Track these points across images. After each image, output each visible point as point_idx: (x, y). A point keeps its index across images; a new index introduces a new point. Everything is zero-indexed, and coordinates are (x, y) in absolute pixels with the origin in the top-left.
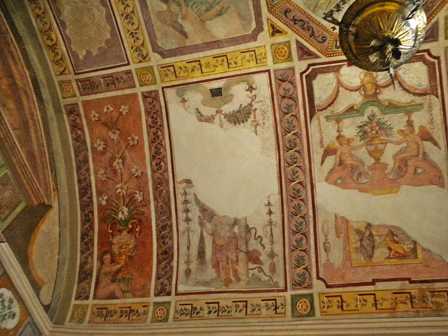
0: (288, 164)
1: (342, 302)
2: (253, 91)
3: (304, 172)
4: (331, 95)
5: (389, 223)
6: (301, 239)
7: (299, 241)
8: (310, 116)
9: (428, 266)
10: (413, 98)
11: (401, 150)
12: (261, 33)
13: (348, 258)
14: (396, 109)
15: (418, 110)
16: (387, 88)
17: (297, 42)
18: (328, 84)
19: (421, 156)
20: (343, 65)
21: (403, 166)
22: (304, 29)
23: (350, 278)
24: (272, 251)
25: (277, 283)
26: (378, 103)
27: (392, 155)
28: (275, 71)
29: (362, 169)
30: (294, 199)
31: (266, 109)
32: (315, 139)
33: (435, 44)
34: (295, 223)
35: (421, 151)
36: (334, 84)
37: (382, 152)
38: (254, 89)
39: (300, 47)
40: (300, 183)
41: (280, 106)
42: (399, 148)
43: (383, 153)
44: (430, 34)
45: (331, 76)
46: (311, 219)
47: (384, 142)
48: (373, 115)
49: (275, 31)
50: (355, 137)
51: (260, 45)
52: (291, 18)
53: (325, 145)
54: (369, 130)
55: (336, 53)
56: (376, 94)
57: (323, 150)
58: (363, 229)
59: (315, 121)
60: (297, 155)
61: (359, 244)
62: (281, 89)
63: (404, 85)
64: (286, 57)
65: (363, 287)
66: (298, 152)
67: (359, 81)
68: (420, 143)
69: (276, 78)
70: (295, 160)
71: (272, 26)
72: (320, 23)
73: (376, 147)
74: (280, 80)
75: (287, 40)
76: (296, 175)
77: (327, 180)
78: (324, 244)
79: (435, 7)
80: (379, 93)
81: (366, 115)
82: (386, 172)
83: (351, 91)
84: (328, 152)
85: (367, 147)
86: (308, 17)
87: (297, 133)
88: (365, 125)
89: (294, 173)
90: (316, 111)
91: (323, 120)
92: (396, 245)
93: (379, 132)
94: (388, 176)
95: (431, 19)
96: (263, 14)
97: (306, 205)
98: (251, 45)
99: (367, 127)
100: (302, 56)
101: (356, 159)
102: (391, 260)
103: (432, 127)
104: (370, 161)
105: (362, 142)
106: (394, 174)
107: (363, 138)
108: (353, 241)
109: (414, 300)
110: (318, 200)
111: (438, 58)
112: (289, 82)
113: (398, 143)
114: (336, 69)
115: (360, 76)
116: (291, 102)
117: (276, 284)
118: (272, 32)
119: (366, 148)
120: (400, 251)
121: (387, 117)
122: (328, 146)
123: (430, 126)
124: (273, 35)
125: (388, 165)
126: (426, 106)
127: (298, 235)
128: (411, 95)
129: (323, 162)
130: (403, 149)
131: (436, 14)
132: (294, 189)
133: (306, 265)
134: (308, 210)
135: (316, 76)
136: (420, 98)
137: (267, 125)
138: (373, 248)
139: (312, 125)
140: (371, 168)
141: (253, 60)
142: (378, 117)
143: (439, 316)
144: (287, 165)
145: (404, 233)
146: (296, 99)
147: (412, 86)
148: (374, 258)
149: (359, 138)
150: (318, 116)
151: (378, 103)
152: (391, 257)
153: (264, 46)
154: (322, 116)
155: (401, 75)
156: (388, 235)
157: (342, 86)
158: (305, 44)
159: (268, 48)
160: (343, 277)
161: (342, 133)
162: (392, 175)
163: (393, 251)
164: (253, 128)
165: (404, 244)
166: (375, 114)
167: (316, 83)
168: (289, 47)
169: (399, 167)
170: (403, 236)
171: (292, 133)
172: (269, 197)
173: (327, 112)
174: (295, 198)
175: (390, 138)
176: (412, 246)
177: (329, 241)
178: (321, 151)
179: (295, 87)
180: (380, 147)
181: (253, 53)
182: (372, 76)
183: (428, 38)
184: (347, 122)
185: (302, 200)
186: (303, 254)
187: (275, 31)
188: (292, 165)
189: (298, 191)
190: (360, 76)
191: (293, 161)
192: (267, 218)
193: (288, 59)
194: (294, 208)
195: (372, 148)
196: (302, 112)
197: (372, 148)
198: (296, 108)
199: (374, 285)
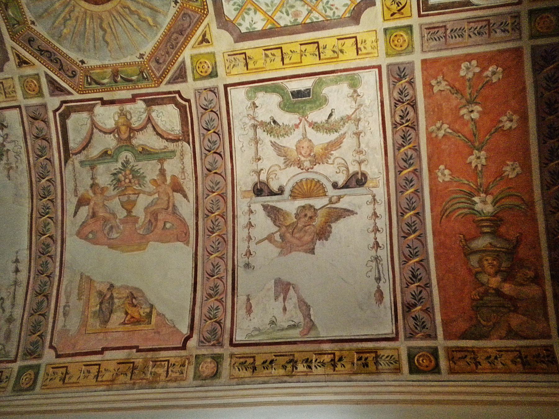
0: (41, 215)
1: (67, 373)
2: (5, 129)
3: (55, 223)
4: (85, 137)
5: (130, 285)
6: (42, 302)
7: (40, 304)
8: (65, 159)
9: (159, 333)
10: (166, 143)
11: (152, 202)
12: (7, 63)
13: (84, 324)
14: (150, 156)
15: (171, 158)
17: (169, 83)
18: (82, 125)
19: (170, 208)
20: (97, 104)
21: (153, 220)
22: (51, 61)
23: (82, 346)
24: (11, 315)
25: (9, 352)
26: (131, 148)
27: (143, 207)
29: (113, 222)
30: (42, 255)
31: (19, 150)
32: (69, 187)
33: (183, 85)
34: (40, 283)
35: (171, 204)
36: (88, 125)
37: (134, 203)
38: (6, 127)
39: (51, 82)
40: (51, 237)
41: (33, 146)
42: (150, 199)
43: (135, 204)
46: (57, 279)
47: (136, 192)
48: (127, 162)
49: (22, 62)
50: (109, 186)
51: (7, 76)
54: (123, 179)
55: (88, 90)
56: (130, 138)
57: (77, 199)
58: (105, 291)
59: (70, 167)
60: (50, 204)
61: (98, 308)
62: (206, 141)
63: (158, 129)
65: (94, 356)
66: (51, 201)
67: (114, 122)
68: (171, 195)
70: (47, 210)
71: (18, 56)
72: (67, 55)
73: (129, 197)
74: (32, 118)
75: (36, 72)
76: (47, 228)
77: (78, 234)
78: (65, 307)
79: (179, 45)
80: (133, 137)
81: (120, 161)
82: (137, 226)
83: (105, 133)
84: (82, 202)
85: (121, 197)
86: (56, 49)
87: (51, 179)
88: (119, 172)
89: (46, 225)
91: (77, 165)
92: (134, 309)
93: (133, 181)
94: (138, 231)
96: (6, 41)
97: (54, 262)
99: (120, 175)
100: (53, 92)
101: (108, 211)
102: (127, 325)
103: (183, 178)
104: (122, 214)
105: (116, 191)
106: (144, 229)
108: (93, 304)
109: (135, 371)
110: (67, 256)
112: (42, 121)
113: (150, 194)
116: (45, 143)
117: (7, 354)
118: (18, 63)
119: (119, 199)
120: (136, 315)
121: (140, 164)
122: (82, 195)
123: (181, 177)
125: (138, 218)
126: (178, 154)
127: (39, 297)
129: (76, 213)
130: (154, 201)
131: (181, 53)
132: (44, 244)
133: (41, 332)
134: (55, 268)
135: (70, 114)
136: (172, 145)
137: (20, 167)
138: (111, 312)
139: (67, 170)
140: (124, 221)
142: (131, 164)
143: (152, 388)
144: (39, 216)
145: (143, 295)
146: (49, 141)
148: (109, 324)
149: (112, 188)
150: (73, 161)
151: (131, 148)
152: (126, 322)
154: (76, 160)
155: (155, 118)
156: (128, 297)
159: (16, 80)
160: (74, 346)
161: (96, 181)
162: (142, 230)
163: (129, 316)
164: (6, 172)
165: (141, 308)
166: (128, 160)
167: (70, 122)
168: (39, 80)
169: (150, 221)
170: (142, 298)
171: (47, 179)
172: (17, 252)
173: (81, 157)
174: (43, 254)
175: (143, 188)
176: (148, 310)
177: (70, 304)
178: (75, 200)
179: (48, 127)
180: (133, 197)
183: (178, 79)
184: (101, 168)
185: (50, 257)
186: (42, 318)
187: (22, 62)
188: (44, 216)
189: (48, 246)
190: (114, 117)
191: (45, 211)
192: (12, 276)
194: (41, 265)
195: (125, 199)
197: (125, 199)
198: (49, 151)
199: (103, 354)
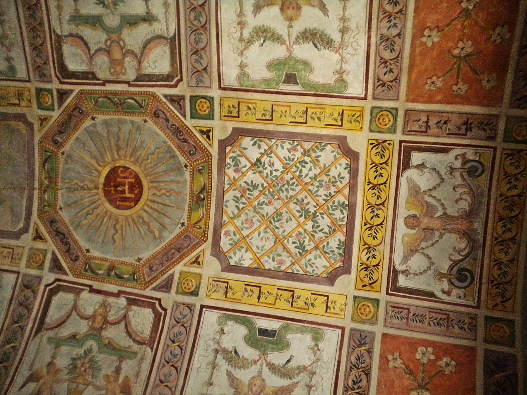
4: (63, 317)
15: (131, 359)
16: (113, 326)
22: (62, 242)
28: (25, 275)
33: (167, 295)
36: (70, 306)
44: (165, 284)
45: (70, 297)
48: (90, 350)
49: (38, 237)
51: (20, 245)
52: (55, 229)
53: (35, 368)
54: (80, 365)
56: (101, 329)
63: (129, 328)
64: (38, 265)
69: (22, 282)
73: (78, 386)
75: (45, 248)
80: (104, 329)
81: (85, 348)
86: (69, 232)
90: (43, 329)
93: (88, 370)
95: (169, 270)
98: (13, 242)
105: (68, 376)
107: (71, 372)
111: (165, 310)
112: (32, 291)
114: (78, 291)
115: (95, 306)
118: (35, 237)
121: (101, 356)
122: (36, 371)
124: (35, 239)
128: (131, 340)
129: (23, 387)
141: (9, 258)
147: (134, 332)
153: (24, 247)
157: (76, 311)
158: (60, 257)
159: (26, 250)
167: (55, 300)
168: (45, 257)
173: (51, 333)
180: (81, 387)
181: (11, 251)
182: (106, 309)
183: (163, 288)
187: (38, 237)
193: (40, 267)
196: (30, 325)
197: (74, 386)
